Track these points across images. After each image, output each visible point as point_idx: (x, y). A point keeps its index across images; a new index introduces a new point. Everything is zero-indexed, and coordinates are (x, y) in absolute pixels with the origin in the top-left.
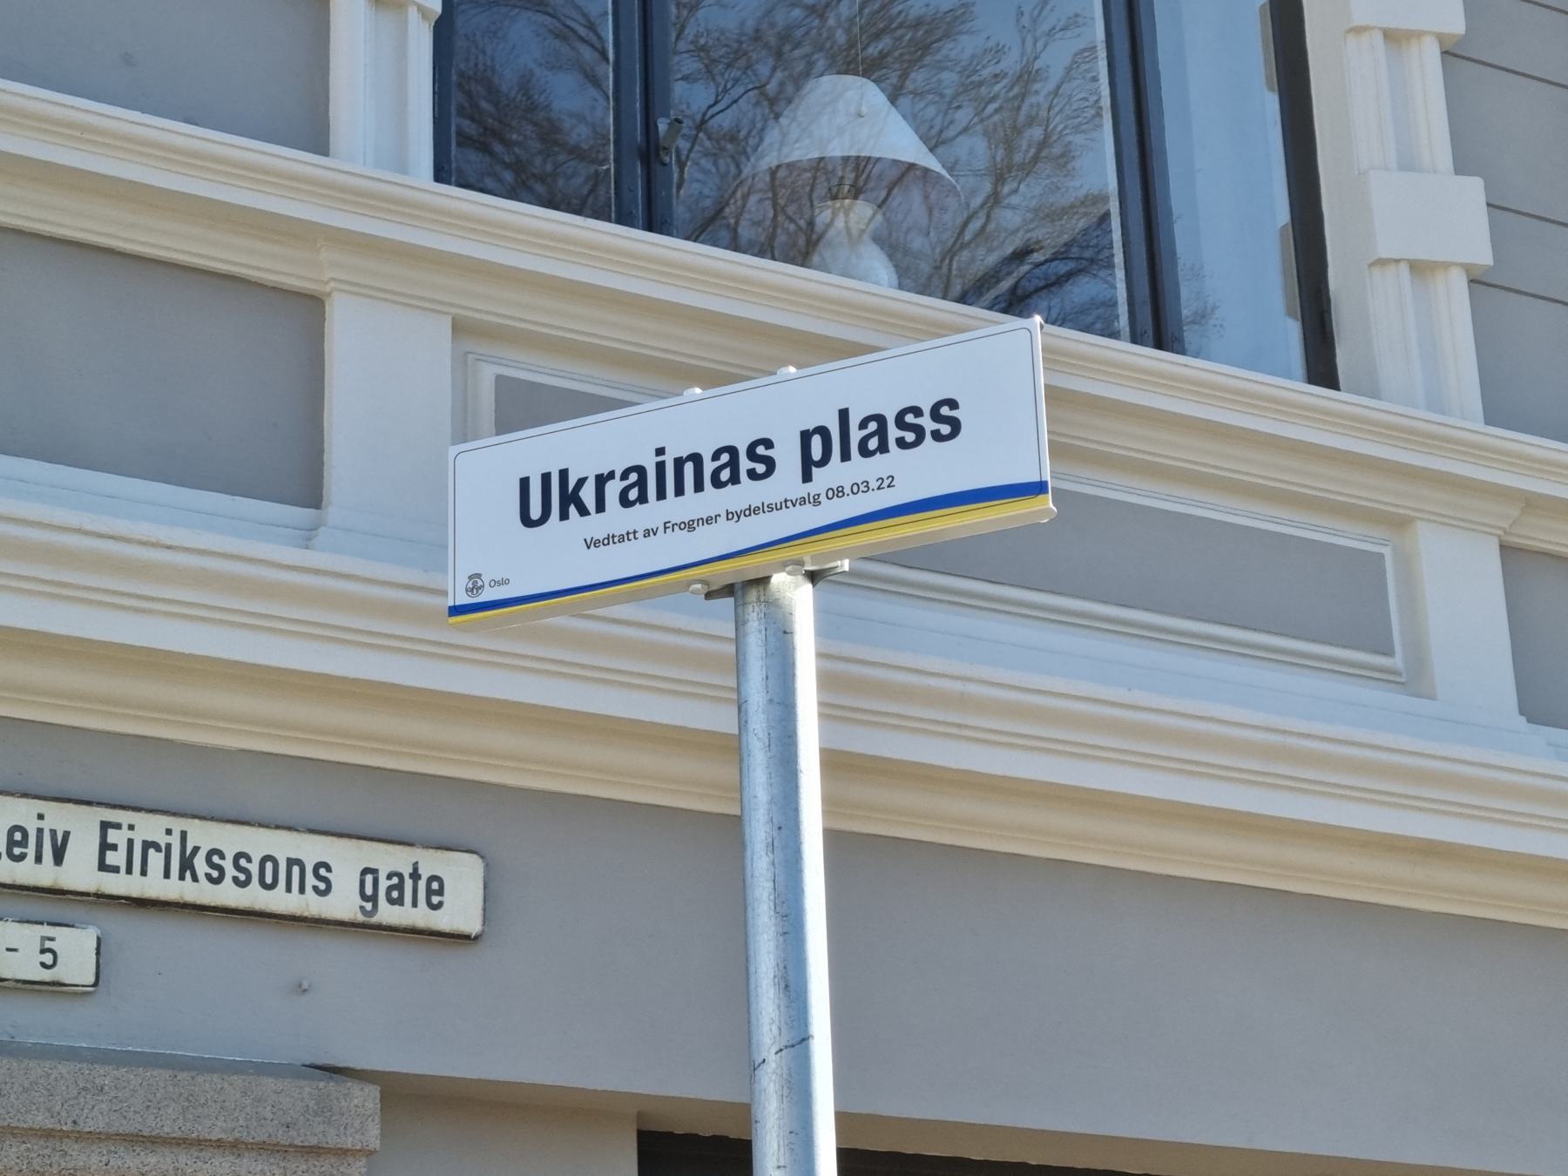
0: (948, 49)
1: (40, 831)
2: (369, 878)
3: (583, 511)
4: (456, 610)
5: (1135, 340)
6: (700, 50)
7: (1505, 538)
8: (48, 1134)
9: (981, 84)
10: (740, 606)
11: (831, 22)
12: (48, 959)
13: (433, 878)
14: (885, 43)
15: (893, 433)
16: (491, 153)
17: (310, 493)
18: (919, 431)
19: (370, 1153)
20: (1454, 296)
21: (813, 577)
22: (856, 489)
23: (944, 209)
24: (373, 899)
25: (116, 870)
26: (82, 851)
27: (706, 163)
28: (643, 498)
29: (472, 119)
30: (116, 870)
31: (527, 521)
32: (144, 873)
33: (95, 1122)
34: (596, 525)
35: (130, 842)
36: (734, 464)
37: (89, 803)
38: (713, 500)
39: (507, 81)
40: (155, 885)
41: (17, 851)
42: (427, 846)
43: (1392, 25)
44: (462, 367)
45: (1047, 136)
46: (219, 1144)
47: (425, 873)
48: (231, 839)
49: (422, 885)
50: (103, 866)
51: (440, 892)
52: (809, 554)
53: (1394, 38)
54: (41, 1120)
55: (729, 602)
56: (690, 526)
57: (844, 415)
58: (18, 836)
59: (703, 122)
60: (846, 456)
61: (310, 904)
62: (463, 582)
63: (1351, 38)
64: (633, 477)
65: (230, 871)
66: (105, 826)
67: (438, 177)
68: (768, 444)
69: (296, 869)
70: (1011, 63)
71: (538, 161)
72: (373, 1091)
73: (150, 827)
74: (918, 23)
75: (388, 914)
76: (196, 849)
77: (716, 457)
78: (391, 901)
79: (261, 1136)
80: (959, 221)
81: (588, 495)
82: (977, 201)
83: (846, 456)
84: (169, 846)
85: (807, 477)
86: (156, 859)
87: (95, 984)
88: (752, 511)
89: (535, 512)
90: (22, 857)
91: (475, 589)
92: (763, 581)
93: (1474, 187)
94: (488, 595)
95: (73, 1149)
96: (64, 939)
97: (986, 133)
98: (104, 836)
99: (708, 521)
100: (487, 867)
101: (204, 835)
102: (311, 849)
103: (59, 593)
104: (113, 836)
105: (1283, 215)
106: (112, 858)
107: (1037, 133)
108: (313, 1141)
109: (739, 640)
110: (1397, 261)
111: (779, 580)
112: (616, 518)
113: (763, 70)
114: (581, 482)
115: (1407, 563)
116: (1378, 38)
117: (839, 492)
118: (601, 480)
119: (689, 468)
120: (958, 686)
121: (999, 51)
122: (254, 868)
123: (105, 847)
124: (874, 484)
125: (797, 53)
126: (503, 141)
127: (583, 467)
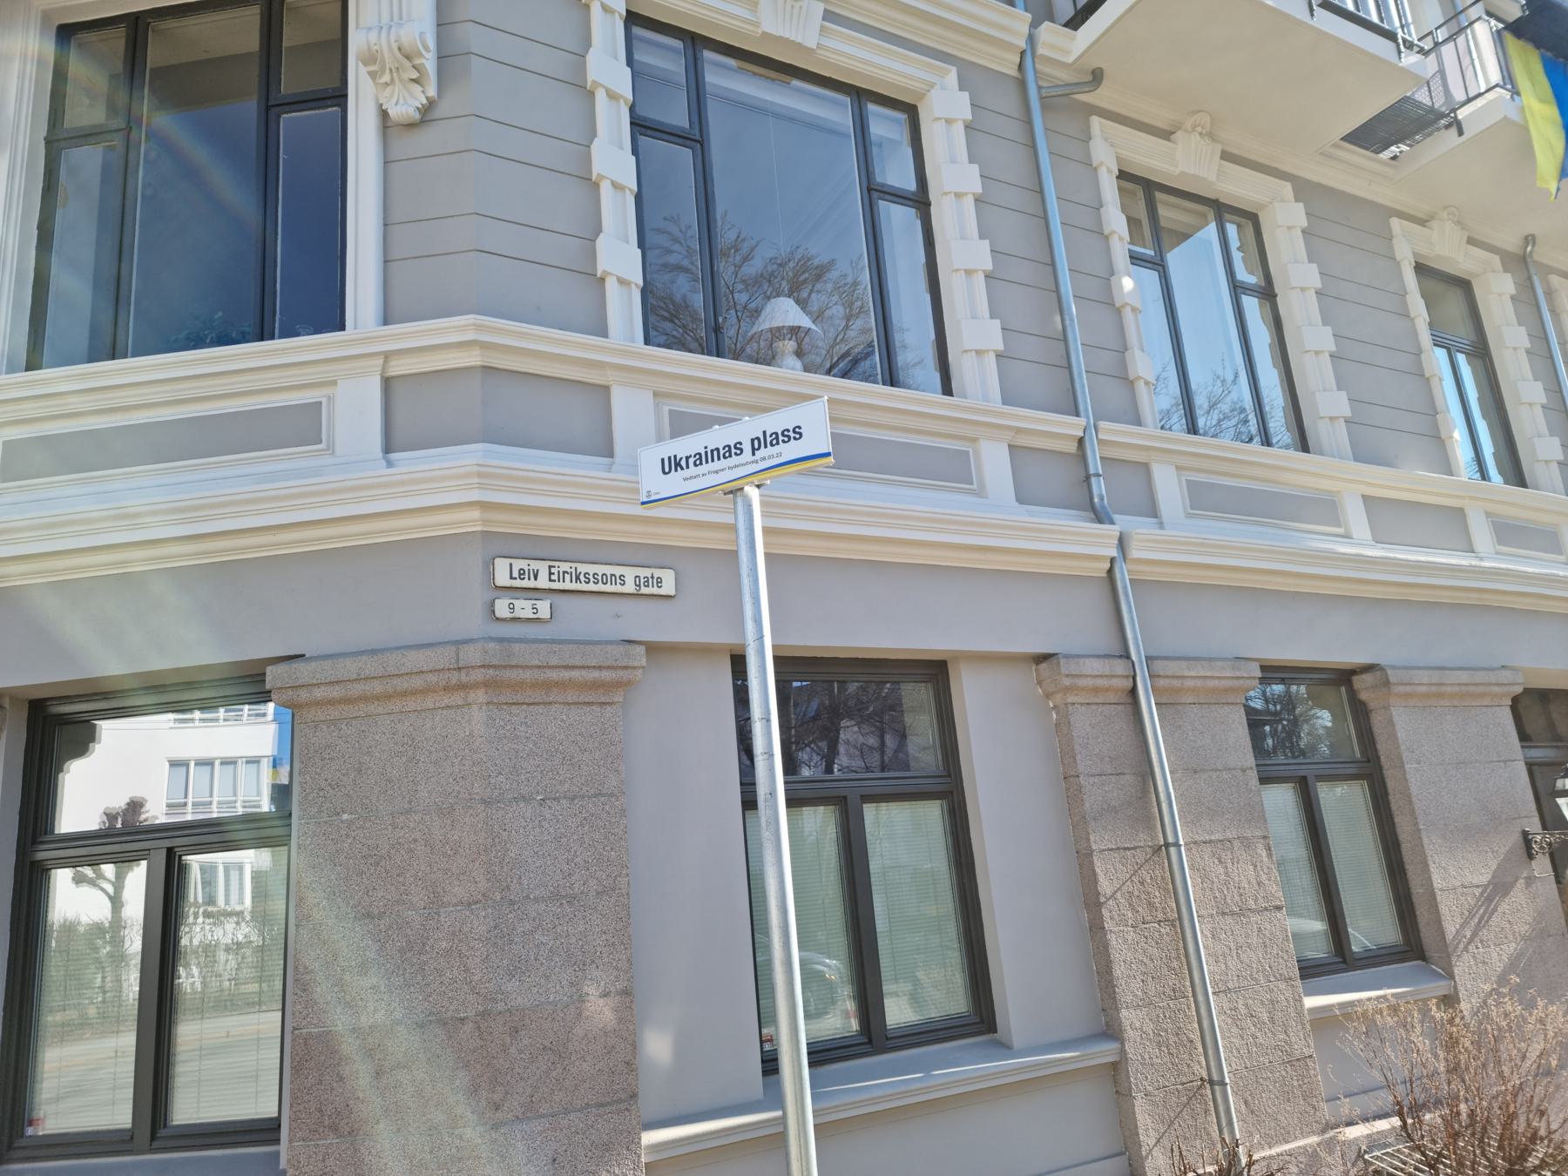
0: (828, 276)
1: (529, 570)
2: (637, 579)
3: (682, 469)
4: (643, 503)
5: (884, 384)
6: (744, 281)
7: (1011, 443)
8: (539, 667)
9: (839, 288)
10: (735, 497)
11: (787, 269)
12: (535, 611)
13: (659, 578)
14: (806, 275)
15: (781, 438)
16: (675, 323)
17: (610, 453)
18: (789, 437)
19: (643, 667)
20: (991, 360)
21: (758, 486)
22: (769, 457)
23: (829, 332)
24: (639, 586)
25: (555, 581)
26: (544, 575)
27: (748, 320)
28: (701, 464)
29: (666, 311)
30: (555, 581)
31: (664, 473)
32: (564, 581)
33: (554, 662)
34: (686, 473)
35: (559, 572)
36: (730, 451)
37: (544, 560)
38: (724, 463)
39: (678, 298)
40: (568, 585)
41: (522, 577)
42: (655, 567)
43: (967, 268)
44: (657, 406)
45: (863, 304)
46: (594, 667)
47: (656, 576)
48: (592, 569)
49: (655, 580)
50: (550, 580)
51: (661, 582)
52: (756, 480)
53: (968, 272)
54: (537, 663)
55: (731, 496)
56: (717, 472)
57: (764, 433)
58: (522, 572)
59: (746, 306)
60: (766, 447)
61: (618, 589)
62: (645, 494)
63: (954, 274)
64: (698, 457)
65: (592, 579)
66: (550, 567)
67: (646, 343)
68: (741, 443)
69: (613, 578)
70: (850, 280)
71: (691, 325)
72: (644, 647)
73: (565, 567)
74: (817, 268)
75: (644, 590)
76: (580, 573)
77: (724, 449)
78: (645, 586)
79: (608, 664)
80: (835, 335)
81: (683, 463)
82: (840, 329)
83: (766, 447)
84: (571, 573)
85: (754, 454)
86: (567, 577)
87: (551, 618)
88: (736, 466)
89: (667, 470)
90: (524, 578)
91: (649, 496)
92: (742, 489)
93: (997, 323)
94: (653, 498)
95: (547, 671)
96: (539, 604)
97: (843, 304)
98: (550, 570)
99: (723, 470)
100: (676, 574)
101: (582, 568)
102: (618, 571)
103: (529, 492)
104: (553, 570)
105: (932, 336)
106: (553, 577)
107: (859, 303)
108: (624, 665)
109: (735, 508)
110: (971, 350)
111: (747, 488)
112: (693, 470)
113: (765, 287)
114: (681, 459)
115: (977, 454)
116: (963, 272)
117: (764, 459)
118: (687, 458)
119: (715, 453)
120: (827, 505)
121: (845, 276)
122: (600, 578)
123: (551, 574)
124: (775, 456)
125: (776, 281)
126: (678, 318)
127: (681, 454)
